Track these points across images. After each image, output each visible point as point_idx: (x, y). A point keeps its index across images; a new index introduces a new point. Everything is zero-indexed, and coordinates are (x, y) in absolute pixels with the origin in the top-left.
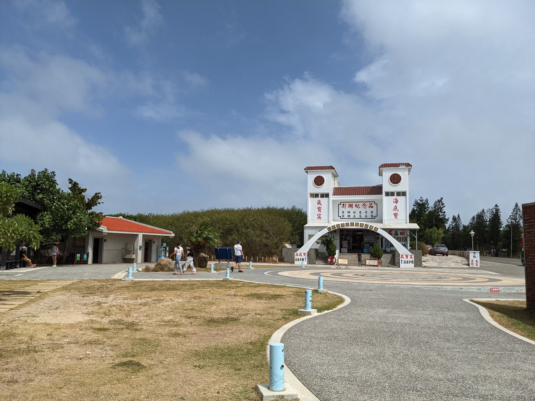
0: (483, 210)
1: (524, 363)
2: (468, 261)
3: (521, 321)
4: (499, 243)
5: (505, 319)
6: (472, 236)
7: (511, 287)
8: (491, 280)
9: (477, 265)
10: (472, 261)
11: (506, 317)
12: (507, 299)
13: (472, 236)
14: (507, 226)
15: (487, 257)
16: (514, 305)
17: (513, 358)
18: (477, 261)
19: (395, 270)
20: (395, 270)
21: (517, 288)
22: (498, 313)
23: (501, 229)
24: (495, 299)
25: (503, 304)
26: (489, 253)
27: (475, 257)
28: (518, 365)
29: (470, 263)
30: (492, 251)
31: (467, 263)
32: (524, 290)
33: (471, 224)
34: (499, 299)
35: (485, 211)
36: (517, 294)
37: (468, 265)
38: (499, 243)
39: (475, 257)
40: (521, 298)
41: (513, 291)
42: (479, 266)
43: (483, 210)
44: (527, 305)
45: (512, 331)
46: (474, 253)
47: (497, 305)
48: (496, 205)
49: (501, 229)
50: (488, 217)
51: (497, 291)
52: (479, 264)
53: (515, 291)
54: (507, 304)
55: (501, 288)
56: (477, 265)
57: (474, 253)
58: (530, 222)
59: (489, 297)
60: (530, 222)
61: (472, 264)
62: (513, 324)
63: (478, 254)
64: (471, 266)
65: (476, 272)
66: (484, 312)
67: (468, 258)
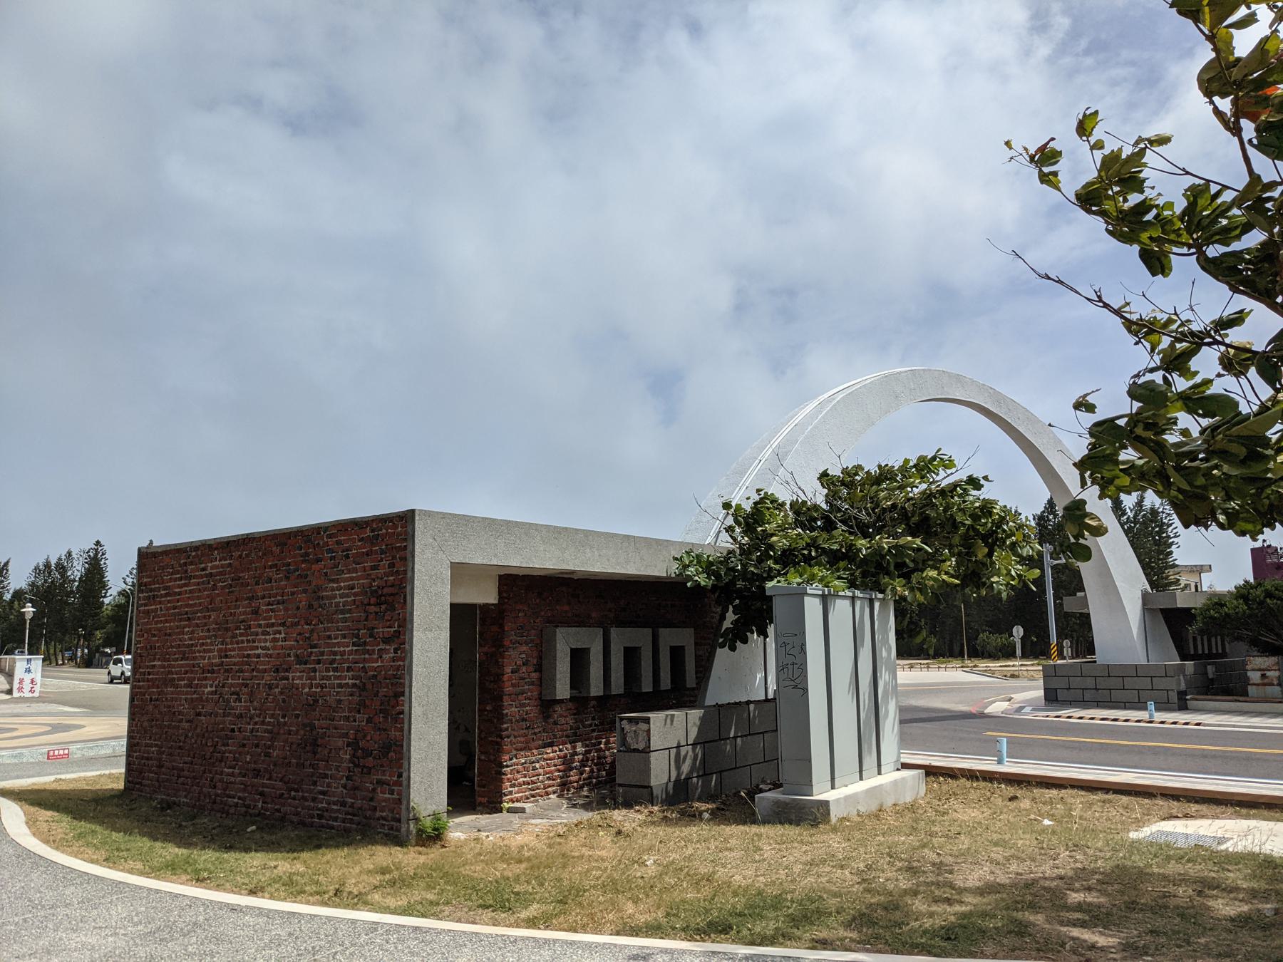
0: (69, 554)
1: (75, 931)
2: (11, 683)
3: (101, 823)
4: (98, 634)
5: (62, 824)
6: (28, 617)
7: (100, 743)
8: (57, 728)
9: (32, 691)
10: (21, 681)
11: (66, 819)
12: (82, 774)
13: (28, 617)
14: (122, 593)
15: (65, 668)
16: (98, 787)
17: (50, 926)
18: (32, 681)
19: (131, 631)
20: (131, 631)
21: (113, 743)
22: (49, 813)
23: (106, 601)
24: (52, 778)
25: (71, 786)
26: (70, 659)
27: (28, 671)
28: (61, 939)
29: (16, 685)
30: (79, 654)
31: (8, 687)
32: (121, 746)
33: (33, 585)
34: (63, 777)
35: (74, 555)
36: (108, 759)
37: (10, 692)
38: (98, 634)
39: (28, 671)
40: (112, 766)
41: (103, 752)
42: (36, 694)
43: (69, 554)
44: (127, 781)
45: (71, 854)
46: (29, 661)
47: (54, 792)
48: (98, 543)
49: (106, 601)
50: (77, 570)
51: (62, 757)
52: (38, 689)
53: (109, 751)
54: (64, 787)
55: (73, 748)
56: (32, 691)
57: (29, 661)
58: (151, 590)
59: (39, 775)
60: (151, 590)
61: (20, 689)
62: (80, 836)
63: (37, 662)
64: (16, 694)
65: (28, 710)
66: (14, 817)
67: (10, 675)
